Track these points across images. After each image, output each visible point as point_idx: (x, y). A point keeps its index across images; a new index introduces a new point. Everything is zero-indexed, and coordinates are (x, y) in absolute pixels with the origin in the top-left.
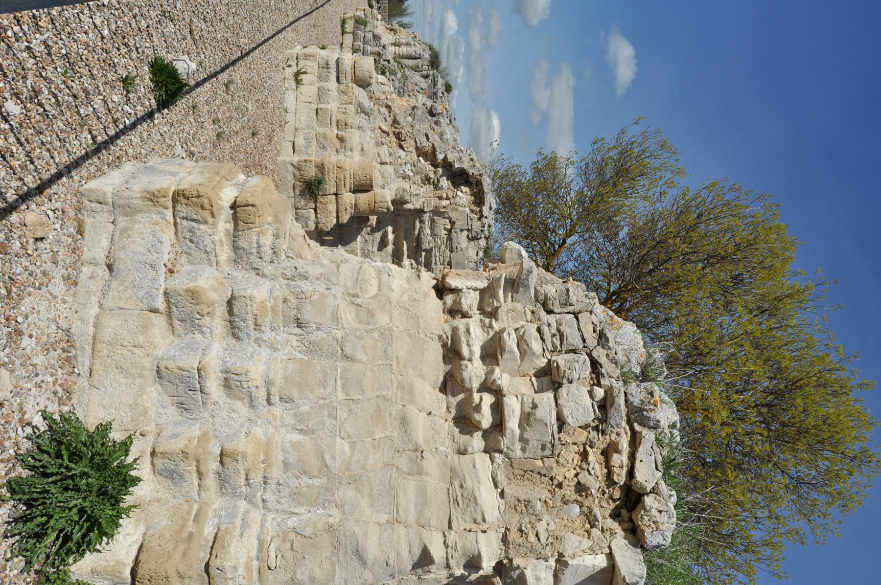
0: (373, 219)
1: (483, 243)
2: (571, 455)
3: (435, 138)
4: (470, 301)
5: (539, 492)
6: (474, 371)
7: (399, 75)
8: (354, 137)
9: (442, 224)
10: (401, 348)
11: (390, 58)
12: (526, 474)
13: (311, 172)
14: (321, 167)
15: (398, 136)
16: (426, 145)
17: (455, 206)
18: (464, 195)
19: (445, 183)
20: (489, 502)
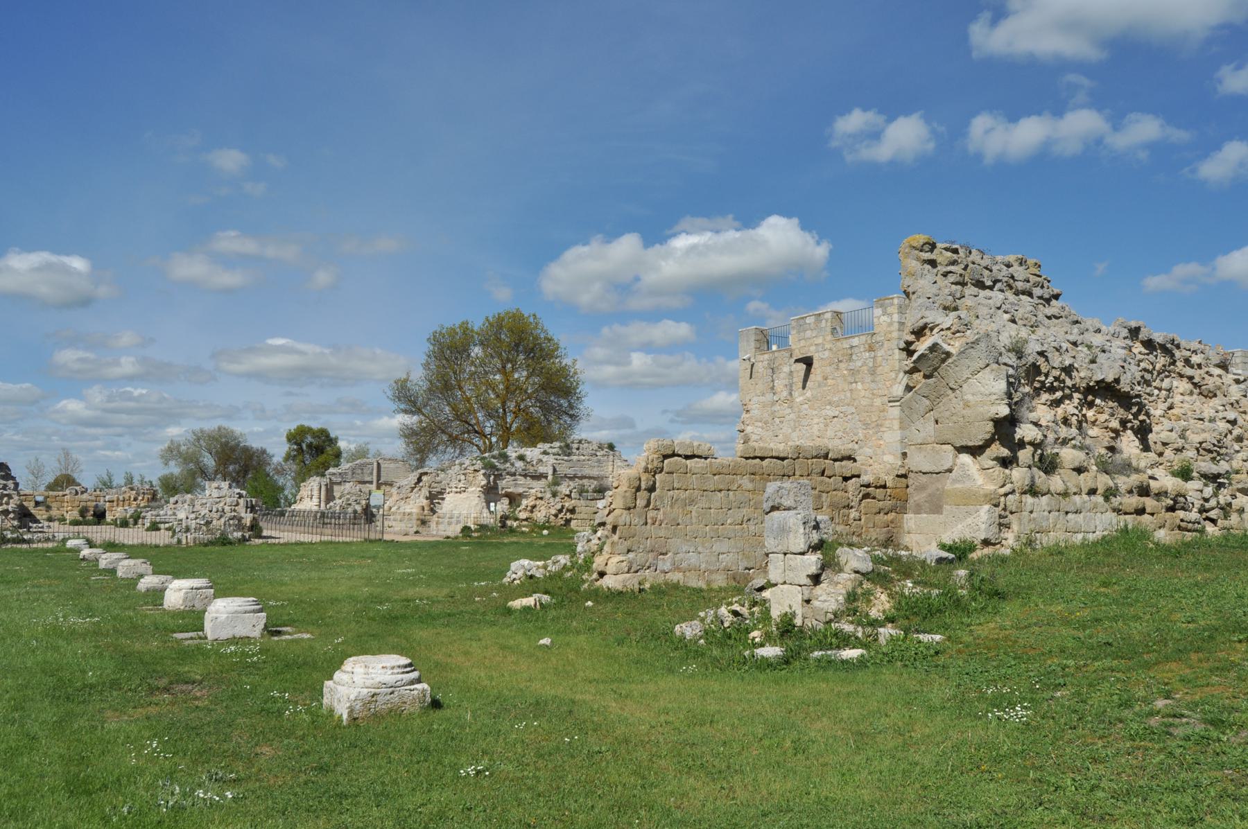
8: (408, 511)
18: (424, 478)
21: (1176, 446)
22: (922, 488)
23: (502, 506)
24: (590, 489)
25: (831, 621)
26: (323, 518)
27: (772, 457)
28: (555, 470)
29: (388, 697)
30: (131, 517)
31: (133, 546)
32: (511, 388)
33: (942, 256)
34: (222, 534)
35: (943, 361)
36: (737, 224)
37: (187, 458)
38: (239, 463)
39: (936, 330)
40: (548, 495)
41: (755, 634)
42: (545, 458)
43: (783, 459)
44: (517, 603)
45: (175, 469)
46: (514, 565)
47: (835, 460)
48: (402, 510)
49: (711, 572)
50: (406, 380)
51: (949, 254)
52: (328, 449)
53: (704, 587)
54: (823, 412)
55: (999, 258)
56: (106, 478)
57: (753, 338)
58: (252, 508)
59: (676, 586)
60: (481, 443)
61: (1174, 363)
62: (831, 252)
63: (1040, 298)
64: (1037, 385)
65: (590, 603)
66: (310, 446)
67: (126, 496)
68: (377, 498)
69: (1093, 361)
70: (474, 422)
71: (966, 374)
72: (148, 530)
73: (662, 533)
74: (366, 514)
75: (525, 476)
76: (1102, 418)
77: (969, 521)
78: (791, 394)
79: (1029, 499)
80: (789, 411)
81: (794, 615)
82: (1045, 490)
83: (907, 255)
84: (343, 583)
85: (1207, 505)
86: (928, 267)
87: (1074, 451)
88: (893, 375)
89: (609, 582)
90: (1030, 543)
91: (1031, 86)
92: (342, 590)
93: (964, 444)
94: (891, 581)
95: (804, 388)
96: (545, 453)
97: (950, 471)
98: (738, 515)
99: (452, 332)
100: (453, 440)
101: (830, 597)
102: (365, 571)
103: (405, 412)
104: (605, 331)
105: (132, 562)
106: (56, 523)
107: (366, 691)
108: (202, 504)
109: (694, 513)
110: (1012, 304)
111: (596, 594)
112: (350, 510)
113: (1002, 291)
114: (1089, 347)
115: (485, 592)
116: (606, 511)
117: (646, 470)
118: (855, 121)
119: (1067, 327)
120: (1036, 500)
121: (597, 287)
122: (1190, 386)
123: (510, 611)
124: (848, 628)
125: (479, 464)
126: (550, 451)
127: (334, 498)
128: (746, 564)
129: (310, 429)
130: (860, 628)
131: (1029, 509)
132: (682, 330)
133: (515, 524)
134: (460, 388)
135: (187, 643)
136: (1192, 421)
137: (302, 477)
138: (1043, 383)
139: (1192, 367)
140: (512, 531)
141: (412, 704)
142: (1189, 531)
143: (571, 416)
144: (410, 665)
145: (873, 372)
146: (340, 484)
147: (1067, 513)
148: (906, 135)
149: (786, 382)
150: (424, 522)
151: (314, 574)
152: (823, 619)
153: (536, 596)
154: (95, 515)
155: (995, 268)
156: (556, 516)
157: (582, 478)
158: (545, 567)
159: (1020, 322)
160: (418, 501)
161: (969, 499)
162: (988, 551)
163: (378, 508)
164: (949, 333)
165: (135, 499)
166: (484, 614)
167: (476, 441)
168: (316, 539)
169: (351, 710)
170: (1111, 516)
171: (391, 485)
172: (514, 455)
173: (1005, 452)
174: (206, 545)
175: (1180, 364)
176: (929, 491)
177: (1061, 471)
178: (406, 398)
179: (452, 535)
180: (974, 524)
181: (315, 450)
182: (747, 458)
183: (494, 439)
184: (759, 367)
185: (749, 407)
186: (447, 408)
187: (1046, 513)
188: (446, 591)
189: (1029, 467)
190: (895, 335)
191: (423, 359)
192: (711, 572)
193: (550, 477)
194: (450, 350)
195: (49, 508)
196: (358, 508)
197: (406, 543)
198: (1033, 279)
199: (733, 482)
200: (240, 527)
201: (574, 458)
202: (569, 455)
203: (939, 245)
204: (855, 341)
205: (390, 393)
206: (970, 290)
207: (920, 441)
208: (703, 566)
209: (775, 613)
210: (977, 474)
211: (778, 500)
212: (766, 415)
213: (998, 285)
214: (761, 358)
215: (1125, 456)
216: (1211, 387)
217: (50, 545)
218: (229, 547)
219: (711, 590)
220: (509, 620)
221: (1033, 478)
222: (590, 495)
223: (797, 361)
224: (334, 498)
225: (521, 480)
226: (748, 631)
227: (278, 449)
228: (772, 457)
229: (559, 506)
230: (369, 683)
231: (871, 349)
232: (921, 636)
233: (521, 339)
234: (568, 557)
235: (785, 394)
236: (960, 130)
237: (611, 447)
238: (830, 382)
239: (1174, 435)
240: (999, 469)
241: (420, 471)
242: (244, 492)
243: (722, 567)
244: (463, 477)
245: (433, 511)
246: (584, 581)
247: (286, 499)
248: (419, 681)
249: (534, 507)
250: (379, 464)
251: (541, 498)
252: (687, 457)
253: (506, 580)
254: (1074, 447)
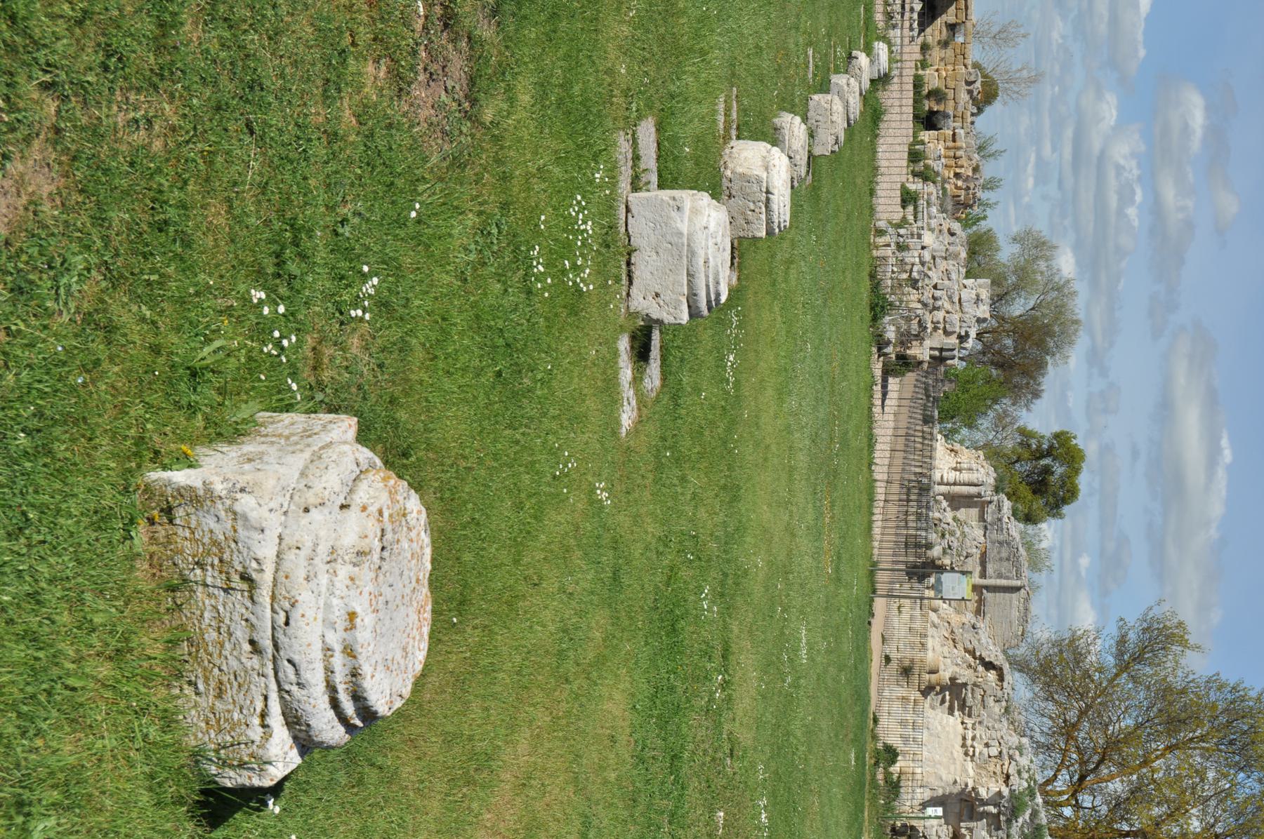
0: (938, 688)
1: (1004, 704)
2: (992, 764)
3: (975, 643)
4: (970, 726)
5: (983, 773)
6: (969, 742)
7: (958, 533)
8: (930, 643)
9: (979, 692)
10: (952, 736)
11: (950, 520)
12: (981, 767)
13: (907, 663)
14: (912, 661)
15: (954, 640)
16: (970, 647)
17: (986, 682)
18: (992, 675)
19: (980, 668)
20: (971, 773)
26: (918, 490)
29: (241, 633)
30: (927, 167)
31: (875, 152)
34: (891, 304)
37: (1024, 277)
38: (1017, 352)
45: (1006, 253)
48: (931, 631)
50: (1183, 643)
52: (1041, 502)
56: (993, 148)
58: (939, 359)
60: (1060, 785)
66: (1047, 471)
67: (964, 162)
68: (957, 586)
70: (1104, 771)
72: (903, 187)
74: (924, 565)
84: (777, 516)
92: (760, 510)
100: (1068, 730)
102: (808, 561)
103: (1122, 641)
105: (841, 125)
106: (919, 57)
107: (267, 551)
108: (948, 273)
112: (933, 537)
125: (1019, 784)
127: (955, 508)
129: (1077, 471)
134: (1170, 748)
135: (624, 146)
137: (992, 453)
141: (215, 721)
144: (368, 714)
146: (982, 518)
151: (802, 460)
154: (932, 113)
160: (945, 661)
163: (937, 587)
165: (957, 175)
168: (880, 473)
169: (197, 499)
171: (978, 612)
174: (872, 276)
178: (1154, 641)
179: (880, 730)
181: (1043, 478)
188: (746, 737)
191: (1230, 677)
195: (944, 44)
196: (936, 552)
197: (867, 640)
200: (906, 339)
205: (1157, 612)
217: (879, 17)
218: (868, 315)
224: (955, 508)
227: (1039, 419)
230: (296, 564)
241: (1006, 667)
242: (970, 344)
244: (994, 751)
245: (927, 691)
247: (954, 431)
248: (305, 743)
250: (1018, 589)
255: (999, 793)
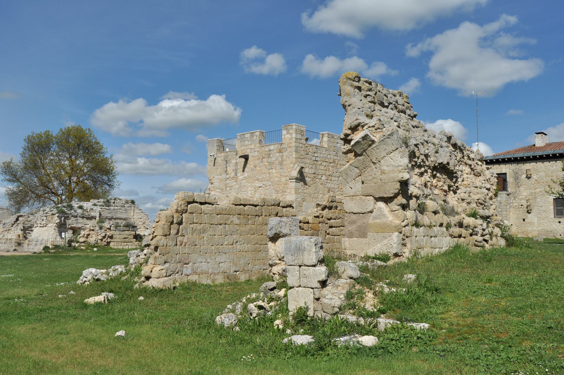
8: (9, 237)
9: (26, 222)
18: (20, 219)
19: (18, 222)
21: (468, 201)
22: (353, 222)
23: (68, 235)
24: (122, 225)
25: (336, 313)
27: (250, 205)
28: (100, 214)
32: (74, 169)
33: (365, 86)
35: (370, 145)
36: (196, 97)
39: (366, 127)
40: (97, 228)
41: (277, 322)
42: (95, 208)
43: (256, 206)
44: (91, 300)
46: (85, 273)
47: (283, 207)
48: (5, 237)
49: (215, 274)
51: (367, 85)
53: (211, 283)
54: (254, 184)
55: (391, 91)
57: (216, 144)
59: (194, 284)
60: (56, 199)
61: (463, 157)
62: (242, 113)
63: (409, 115)
64: (414, 164)
65: (141, 298)
69: (437, 152)
71: (384, 154)
73: (186, 251)
75: (83, 218)
76: (440, 184)
77: (385, 242)
78: (236, 175)
79: (415, 229)
80: (235, 183)
81: (307, 309)
82: (422, 224)
83: (345, 83)
85: (484, 233)
86: (357, 90)
87: (431, 201)
88: (292, 165)
89: (153, 283)
90: (416, 254)
91: (331, 44)
93: (381, 196)
94: (372, 283)
95: (243, 171)
96: (95, 205)
97: (371, 212)
98: (231, 239)
99: (40, 136)
100: (38, 197)
101: (334, 296)
103: (9, 180)
104: (125, 146)
109: (205, 238)
110: (397, 117)
111: (144, 291)
113: (392, 109)
114: (434, 144)
115: (65, 291)
116: (151, 237)
117: (177, 211)
118: (253, 52)
119: (422, 133)
120: (418, 229)
121: (121, 124)
122: (470, 170)
123: (86, 306)
124: (352, 319)
125: (55, 211)
126: (98, 204)
128: (235, 269)
130: (361, 319)
131: (415, 234)
132: (165, 148)
133: (77, 245)
134: (44, 168)
136: (473, 188)
138: (416, 162)
139: (470, 160)
140: (75, 248)
142: (479, 246)
143: (109, 185)
145: (281, 164)
147: (431, 237)
148: (275, 62)
149: (234, 168)
150: (19, 244)
152: (330, 311)
153: (104, 294)
155: (389, 96)
156: (102, 240)
157: (115, 219)
158: (108, 274)
159: (401, 128)
161: (385, 229)
162: (397, 260)
164: (373, 129)
166: (67, 308)
167: (53, 198)
170: (449, 238)
172: (76, 206)
173: (404, 201)
175: (466, 158)
176: (358, 224)
177: (427, 213)
178: (10, 172)
179: (38, 252)
180: (390, 243)
182: (236, 205)
183: (64, 197)
184: (219, 160)
185: (213, 181)
186: (35, 179)
187: (422, 237)
188: (36, 291)
189: (415, 210)
190: (293, 144)
191: (21, 151)
192: (215, 274)
193: (98, 218)
194: (38, 147)
197: (8, 257)
198: (406, 104)
199: (228, 219)
201: (112, 208)
202: (109, 206)
203: (362, 79)
204: (272, 147)
206: (378, 107)
207: (352, 194)
208: (210, 271)
209: (293, 307)
210: (388, 214)
211: (279, 229)
212: (222, 185)
213: (391, 106)
214: (220, 155)
215: (451, 205)
216: (479, 170)
219: (216, 286)
220: (87, 313)
221: (417, 216)
222: (122, 228)
223: (241, 157)
225: (81, 220)
226: (272, 320)
228: (250, 205)
229: (103, 235)
231: (280, 151)
232: (414, 325)
233: (81, 142)
234: (123, 266)
235: (233, 174)
236: (300, 61)
237: (133, 202)
238: (258, 168)
239: (467, 195)
240: (401, 211)
241: (18, 214)
243: (221, 271)
244: (45, 218)
245: (26, 238)
246: (136, 283)
249: (89, 235)
251: (93, 230)
252: (201, 204)
253: (79, 282)
254: (431, 199)
255: (58, 217)
